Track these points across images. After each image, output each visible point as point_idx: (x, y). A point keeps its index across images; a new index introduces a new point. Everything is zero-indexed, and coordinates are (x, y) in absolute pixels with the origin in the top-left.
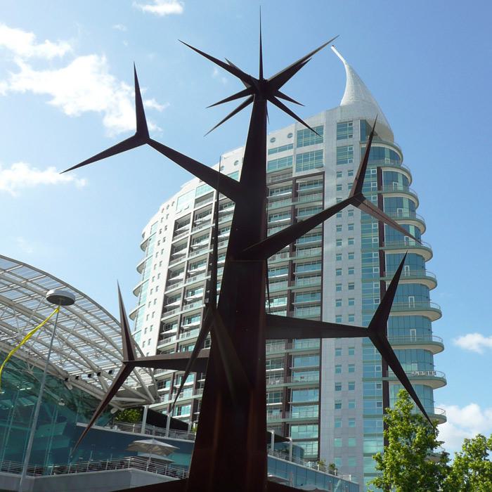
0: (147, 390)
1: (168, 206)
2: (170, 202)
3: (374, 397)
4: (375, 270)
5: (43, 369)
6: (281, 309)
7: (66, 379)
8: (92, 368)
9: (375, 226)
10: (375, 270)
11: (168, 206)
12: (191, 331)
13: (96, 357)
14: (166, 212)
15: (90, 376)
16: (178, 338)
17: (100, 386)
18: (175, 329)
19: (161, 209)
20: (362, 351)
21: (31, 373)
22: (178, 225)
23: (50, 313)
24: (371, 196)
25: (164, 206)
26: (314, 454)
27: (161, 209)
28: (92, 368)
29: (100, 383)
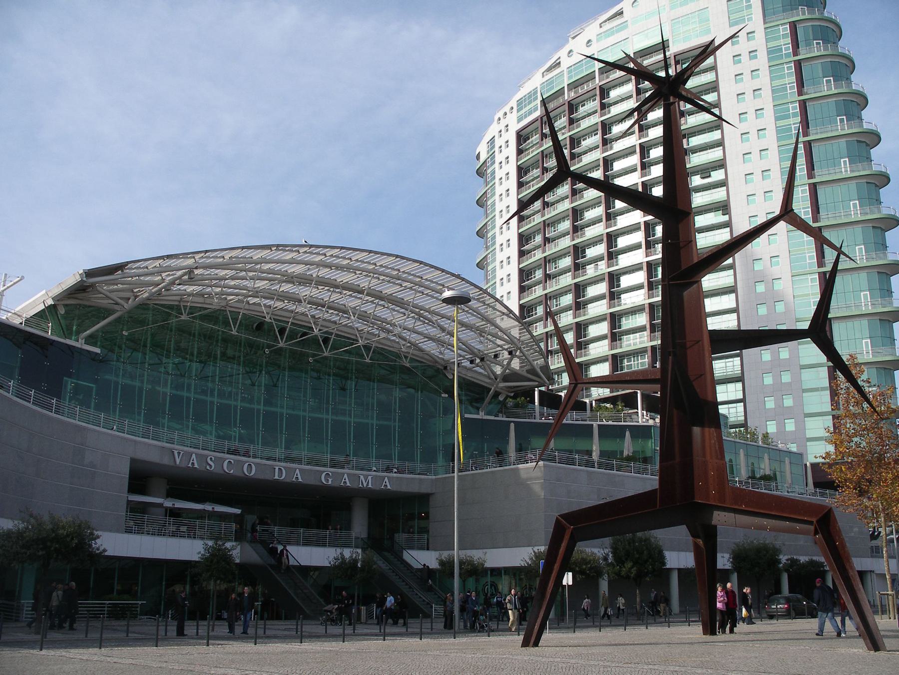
0: (539, 370)
1: (506, 114)
2: (507, 109)
3: (808, 295)
4: (791, 88)
5: (287, 320)
6: (631, 170)
7: (445, 368)
8: (472, 353)
9: (794, 108)
10: (791, 88)
11: (506, 114)
12: (561, 277)
13: (481, 342)
14: (503, 122)
15: (472, 362)
16: (545, 289)
17: (482, 371)
18: (539, 274)
19: (496, 118)
20: (810, 351)
21: (408, 365)
22: (522, 137)
23: (452, 310)
24: (802, 206)
25: (500, 114)
26: (739, 419)
27: (496, 118)
28: (472, 353)
29: (484, 369)
